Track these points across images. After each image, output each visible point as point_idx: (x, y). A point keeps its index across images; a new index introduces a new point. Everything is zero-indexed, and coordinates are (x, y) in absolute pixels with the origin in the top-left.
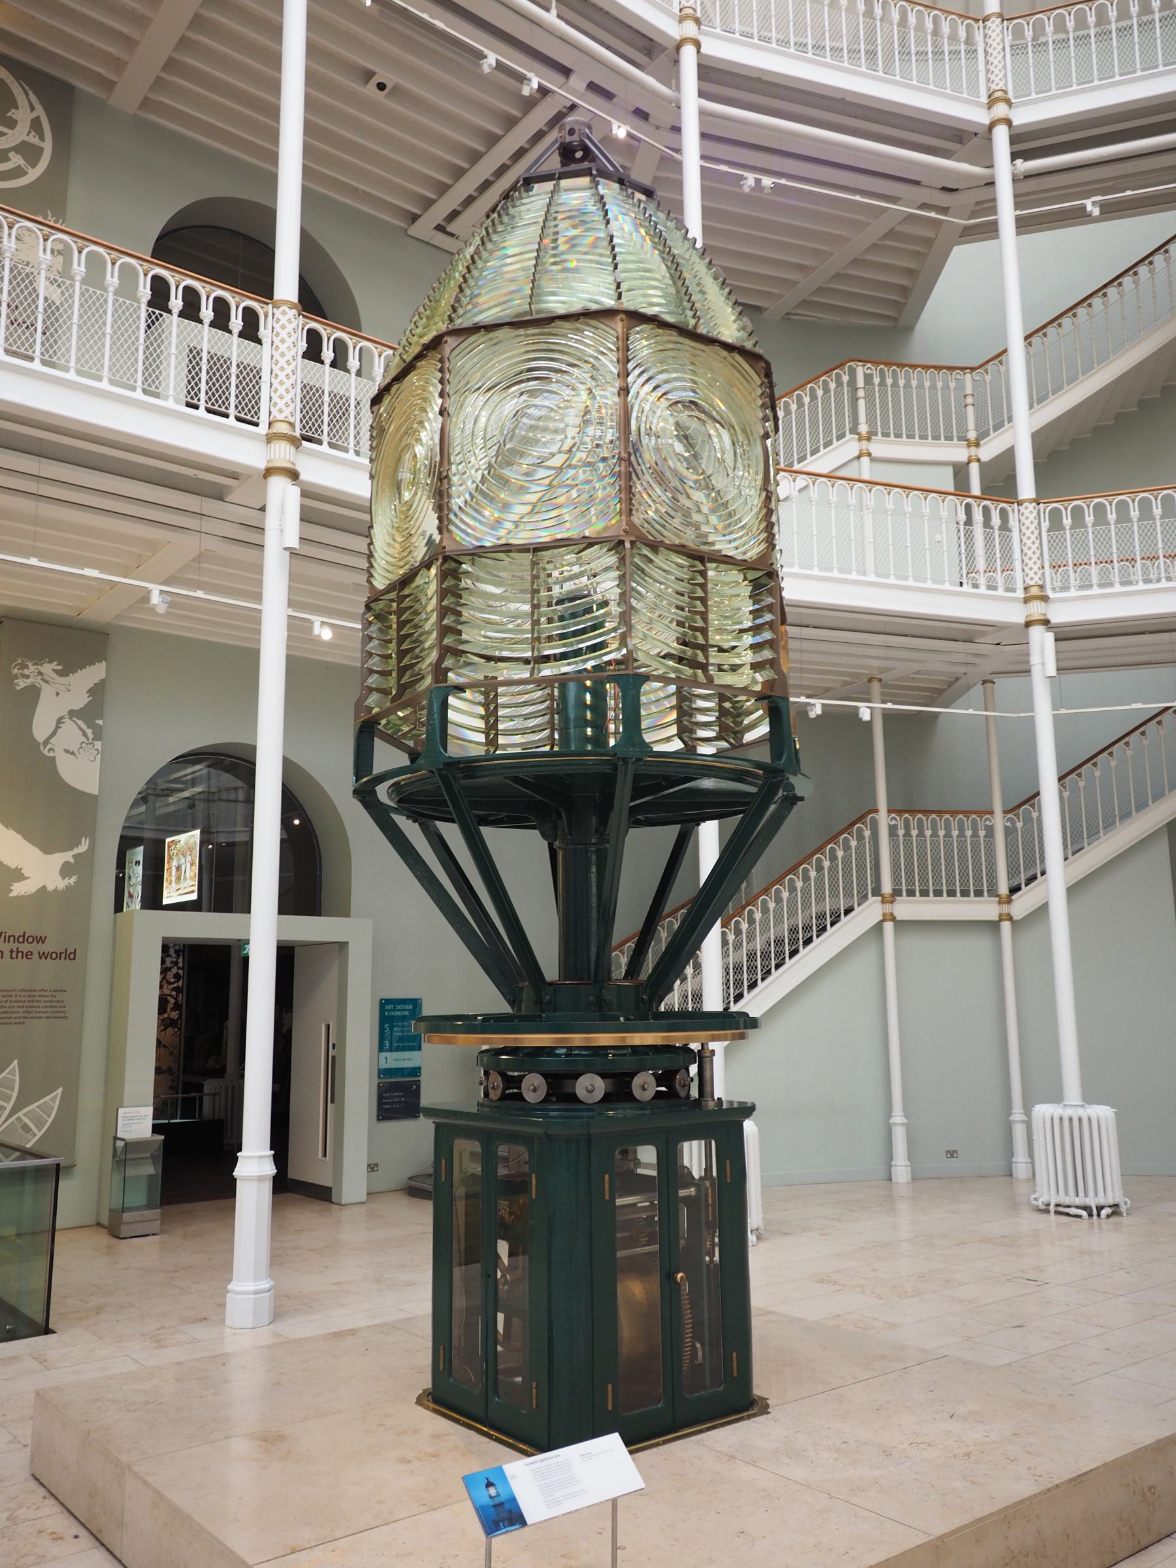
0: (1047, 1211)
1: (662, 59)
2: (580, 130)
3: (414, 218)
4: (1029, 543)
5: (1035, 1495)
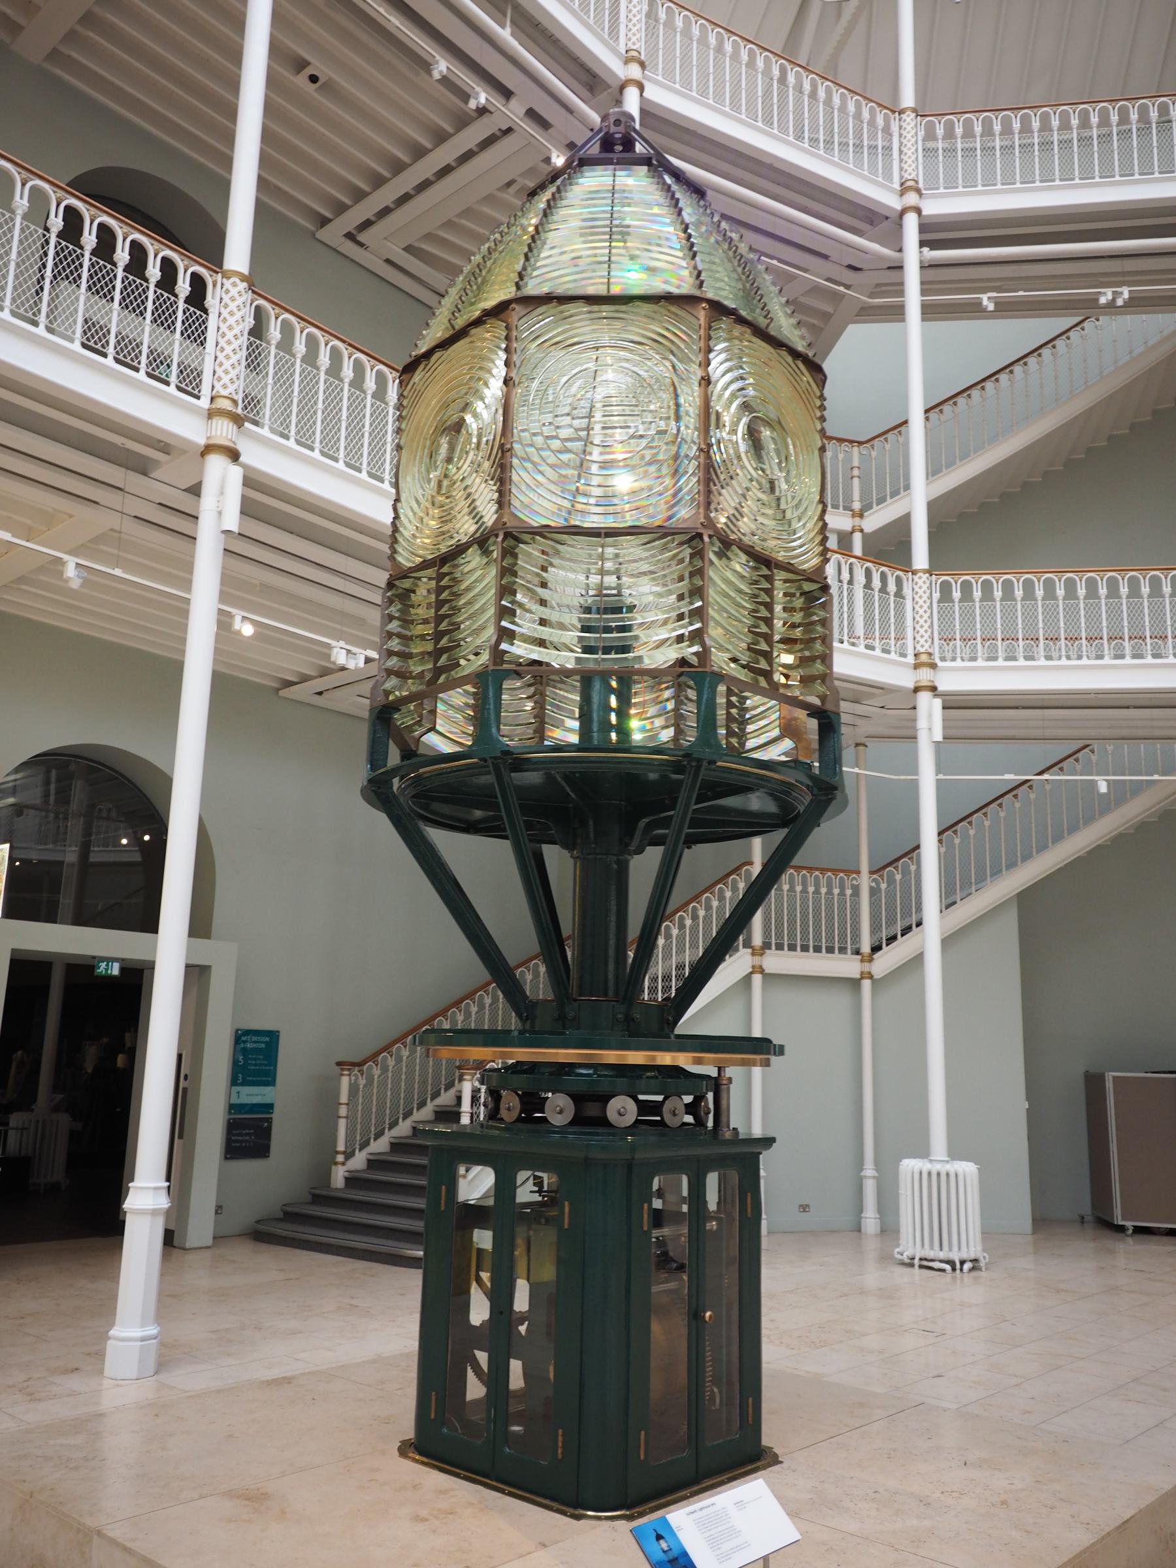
0: (912, 1265)
1: (604, 96)
2: (626, 122)
3: (324, 222)
4: (921, 612)
5: (1093, 1544)
